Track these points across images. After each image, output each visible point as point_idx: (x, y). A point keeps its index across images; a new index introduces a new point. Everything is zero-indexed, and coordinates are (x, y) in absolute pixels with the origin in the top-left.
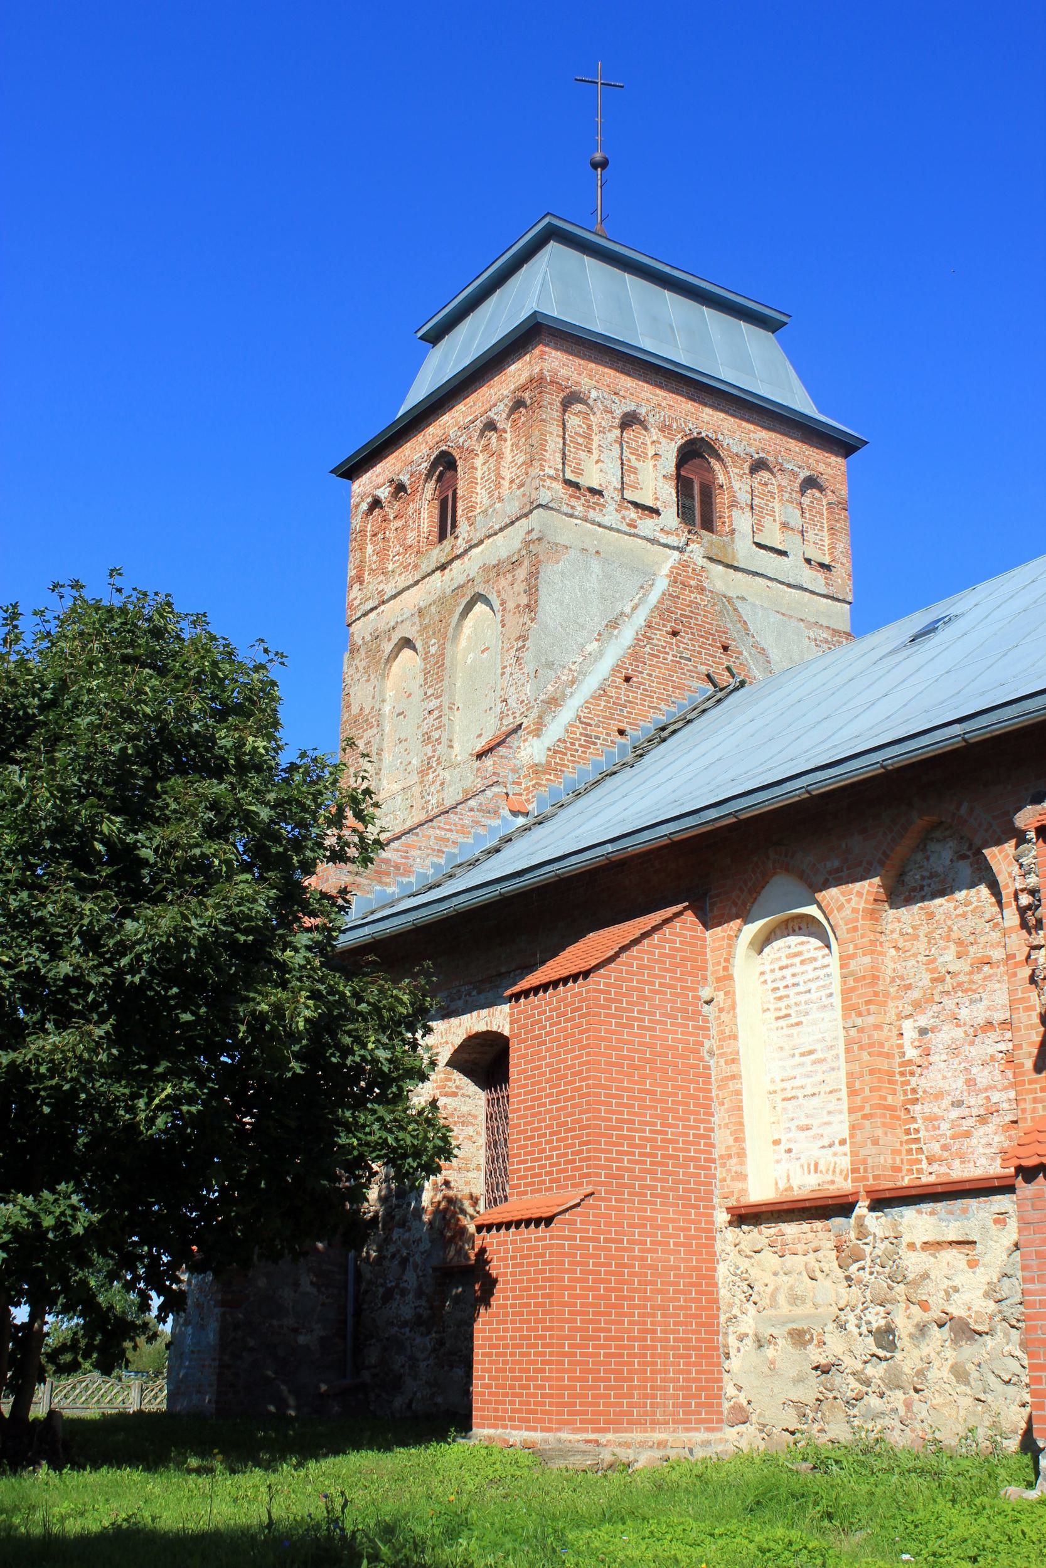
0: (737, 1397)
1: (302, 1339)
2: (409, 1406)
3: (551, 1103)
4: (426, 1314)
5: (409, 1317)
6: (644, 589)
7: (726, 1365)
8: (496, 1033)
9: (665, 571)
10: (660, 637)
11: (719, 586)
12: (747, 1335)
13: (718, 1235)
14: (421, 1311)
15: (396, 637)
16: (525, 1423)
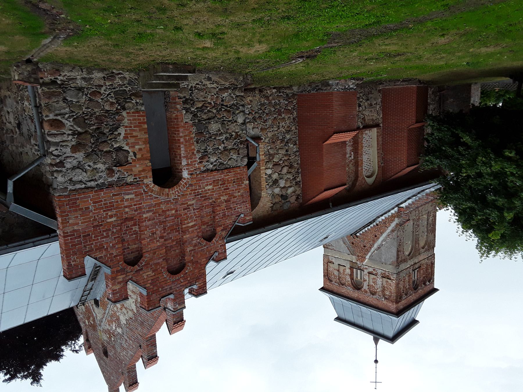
6: (371, 256)
10: (368, 245)
11: (354, 257)
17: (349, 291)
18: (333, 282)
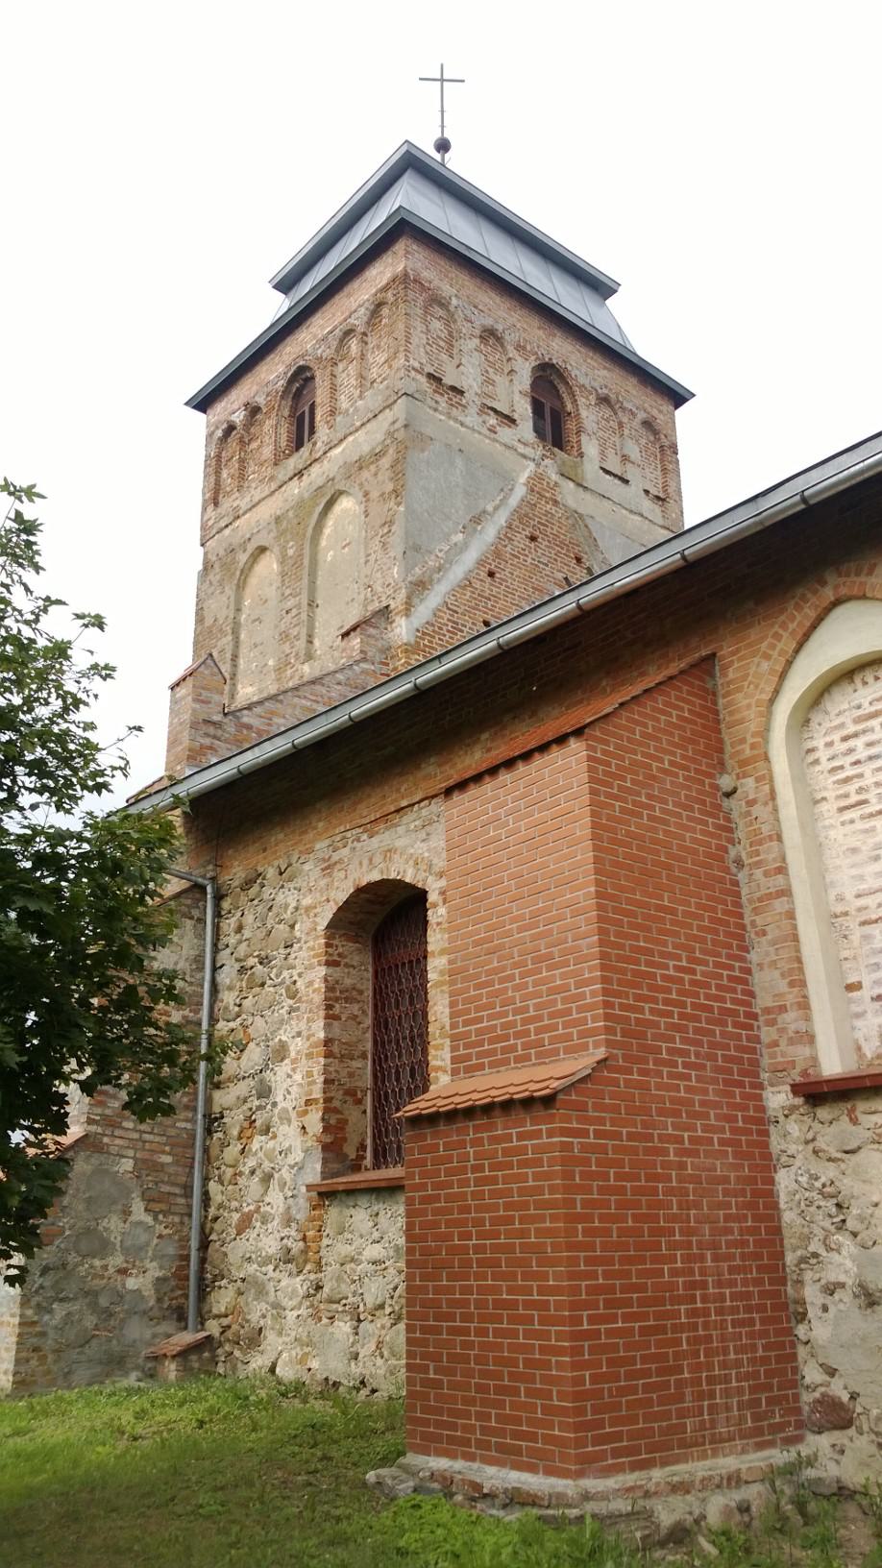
0: (828, 1385)
1: (132, 1283)
2: (272, 1370)
3: (520, 930)
4: (297, 1247)
5: (271, 1251)
6: (507, 490)
7: (801, 1331)
8: (394, 881)
9: (523, 479)
10: (520, 540)
11: (571, 503)
12: (842, 1285)
13: (772, 1129)
14: (289, 1243)
15: (251, 547)
16: (509, 1456)
17: (584, 370)
18: (641, 416)
